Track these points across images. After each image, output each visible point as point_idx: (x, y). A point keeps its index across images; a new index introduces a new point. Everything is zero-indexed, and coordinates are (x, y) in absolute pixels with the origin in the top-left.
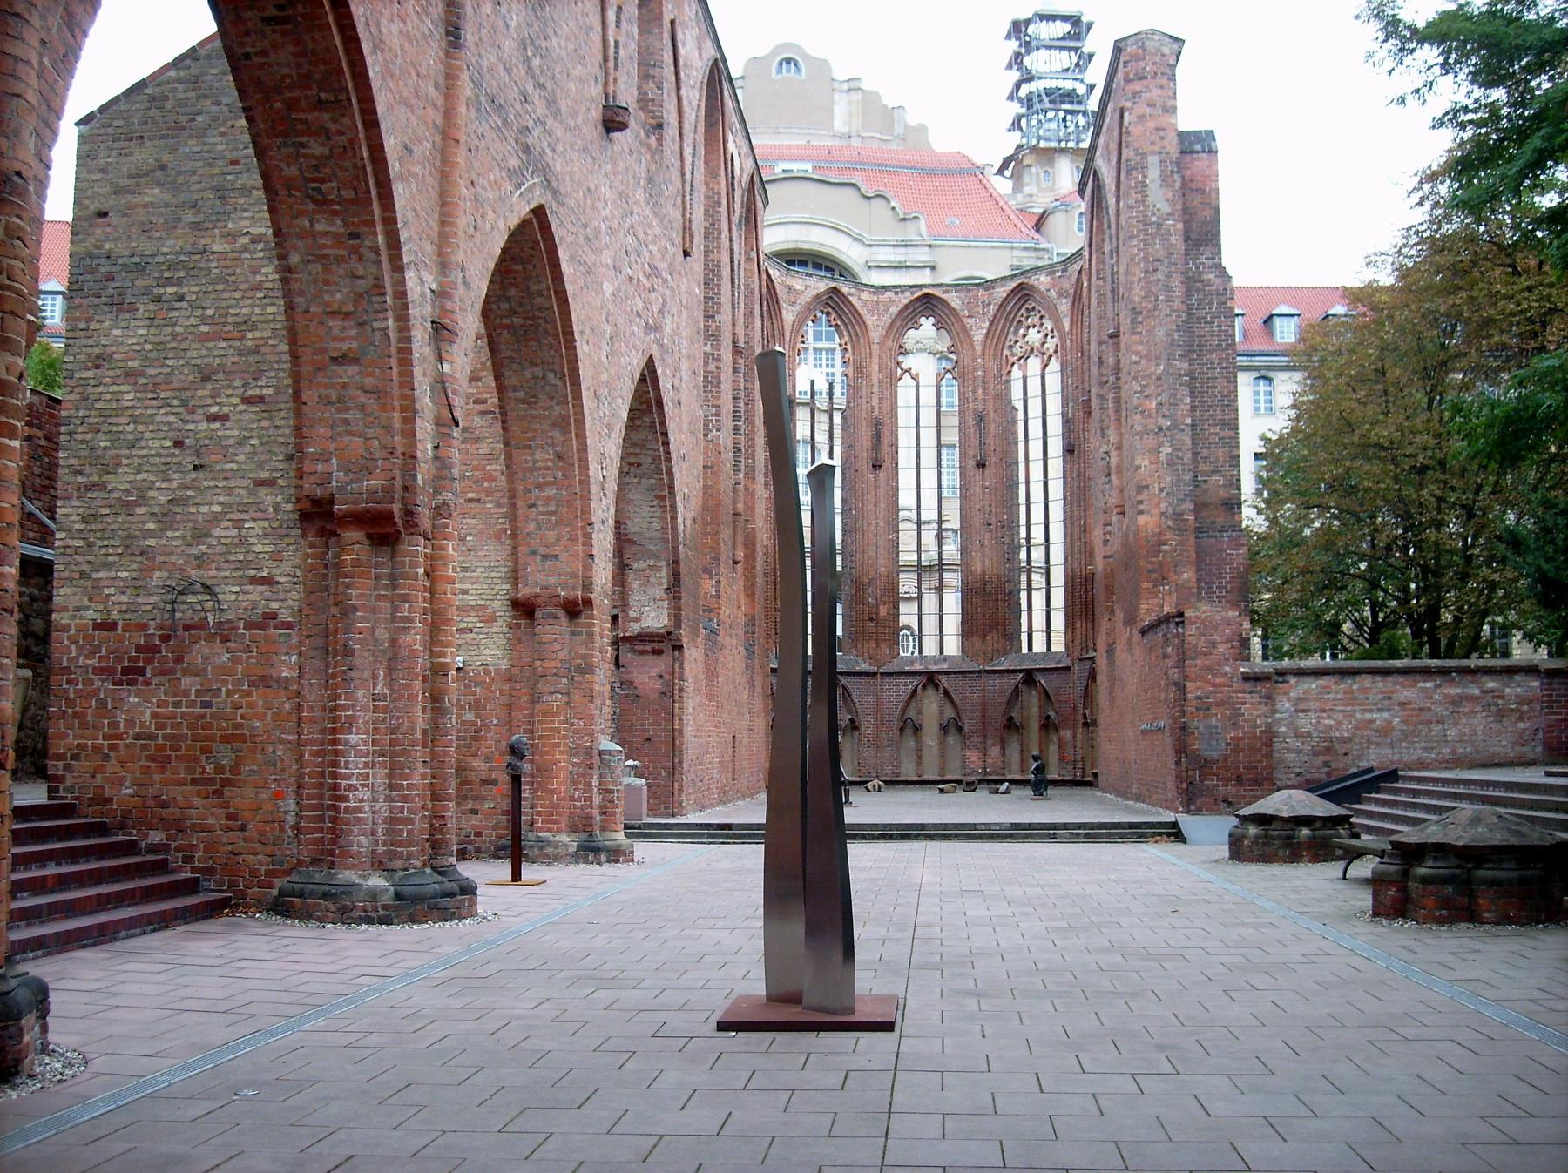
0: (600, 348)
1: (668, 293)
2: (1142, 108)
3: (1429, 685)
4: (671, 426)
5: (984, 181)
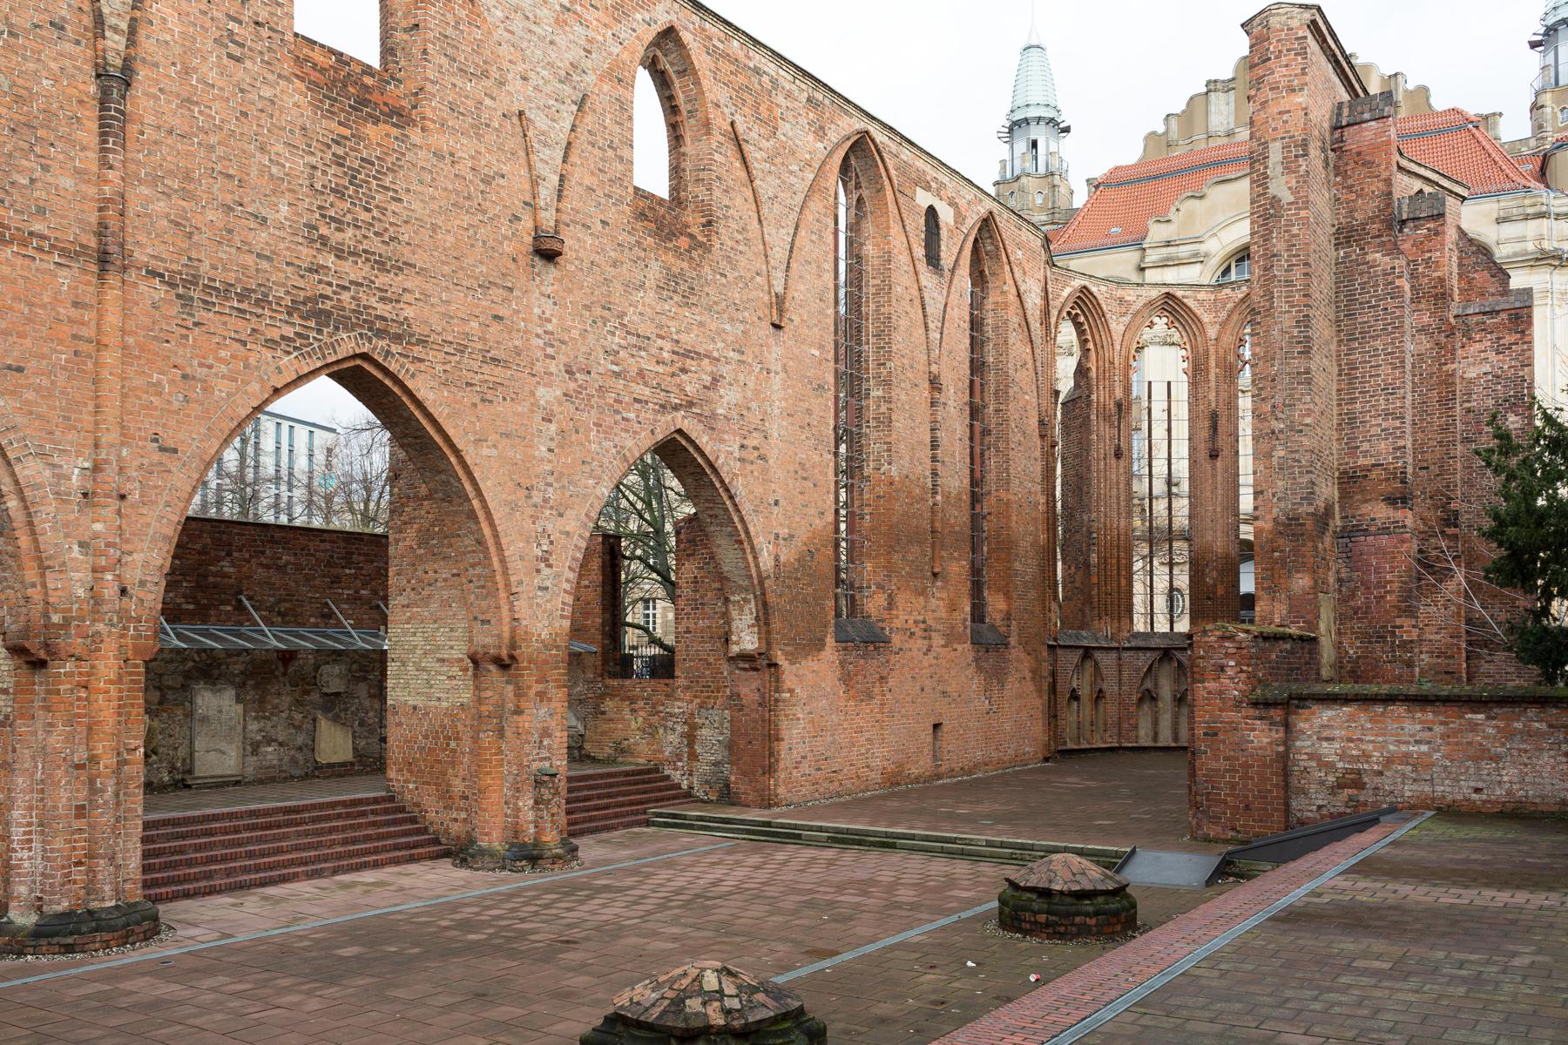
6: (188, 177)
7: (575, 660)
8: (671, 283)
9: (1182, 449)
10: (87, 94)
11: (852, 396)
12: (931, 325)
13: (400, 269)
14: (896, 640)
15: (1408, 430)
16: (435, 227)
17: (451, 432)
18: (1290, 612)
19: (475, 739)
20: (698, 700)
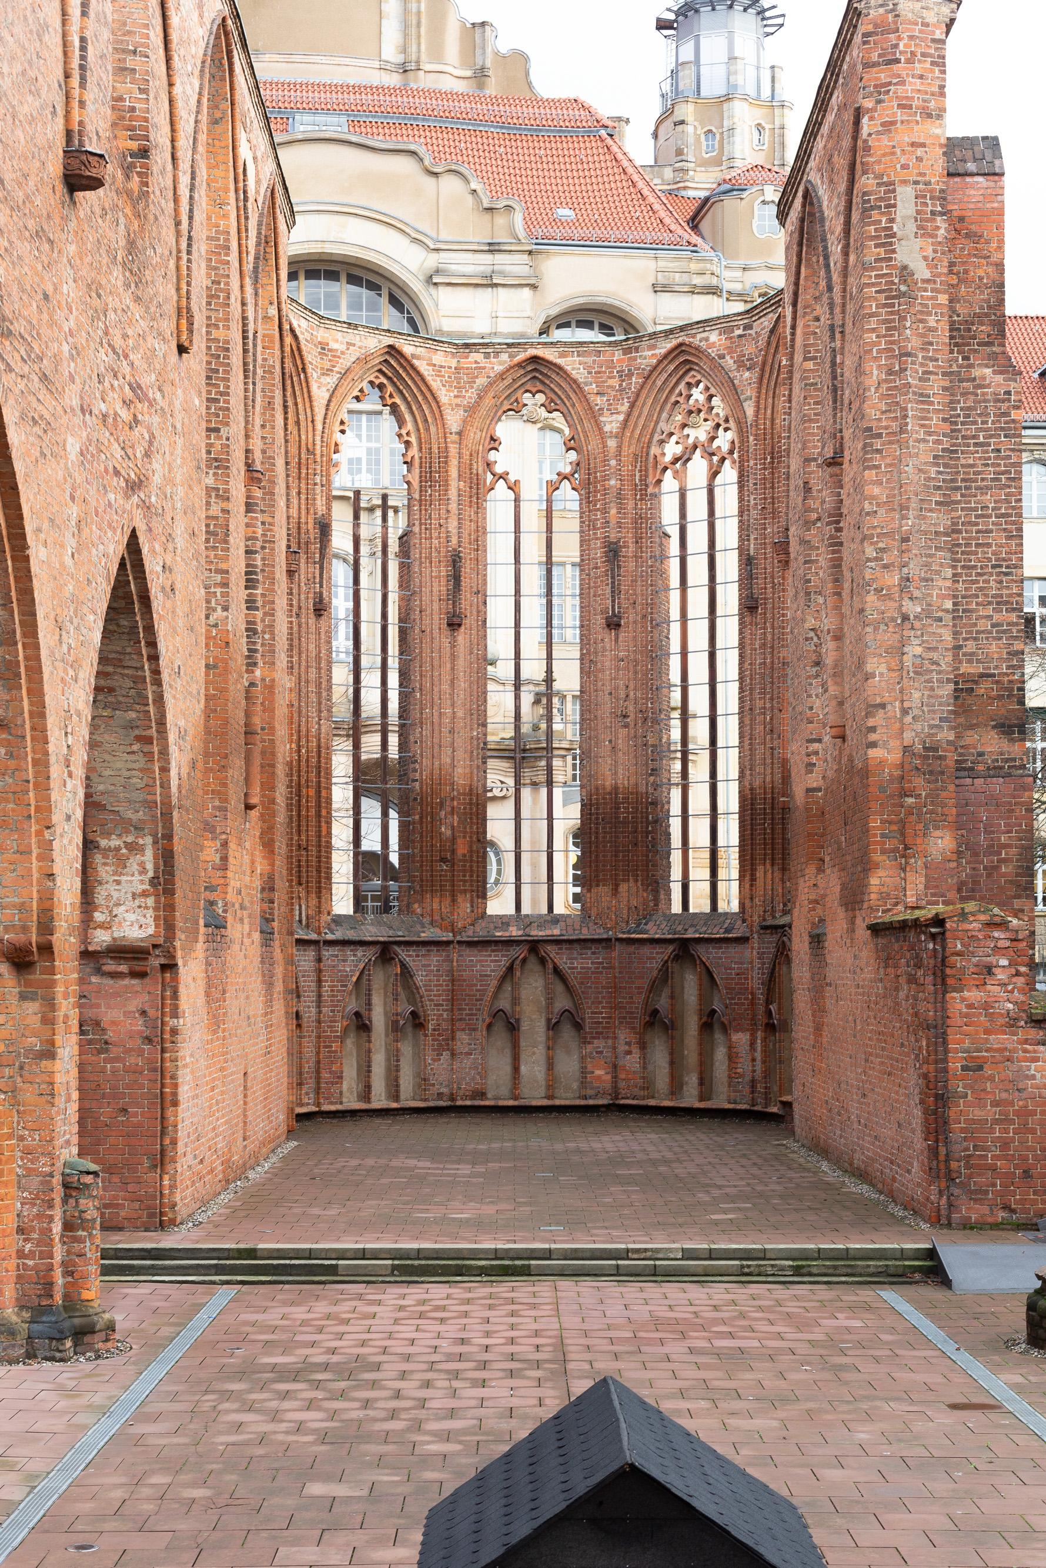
0: (62, 546)
1: (156, 419)
2: (890, 110)
4: (162, 630)
5: (615, 149)
18: (926, 887)
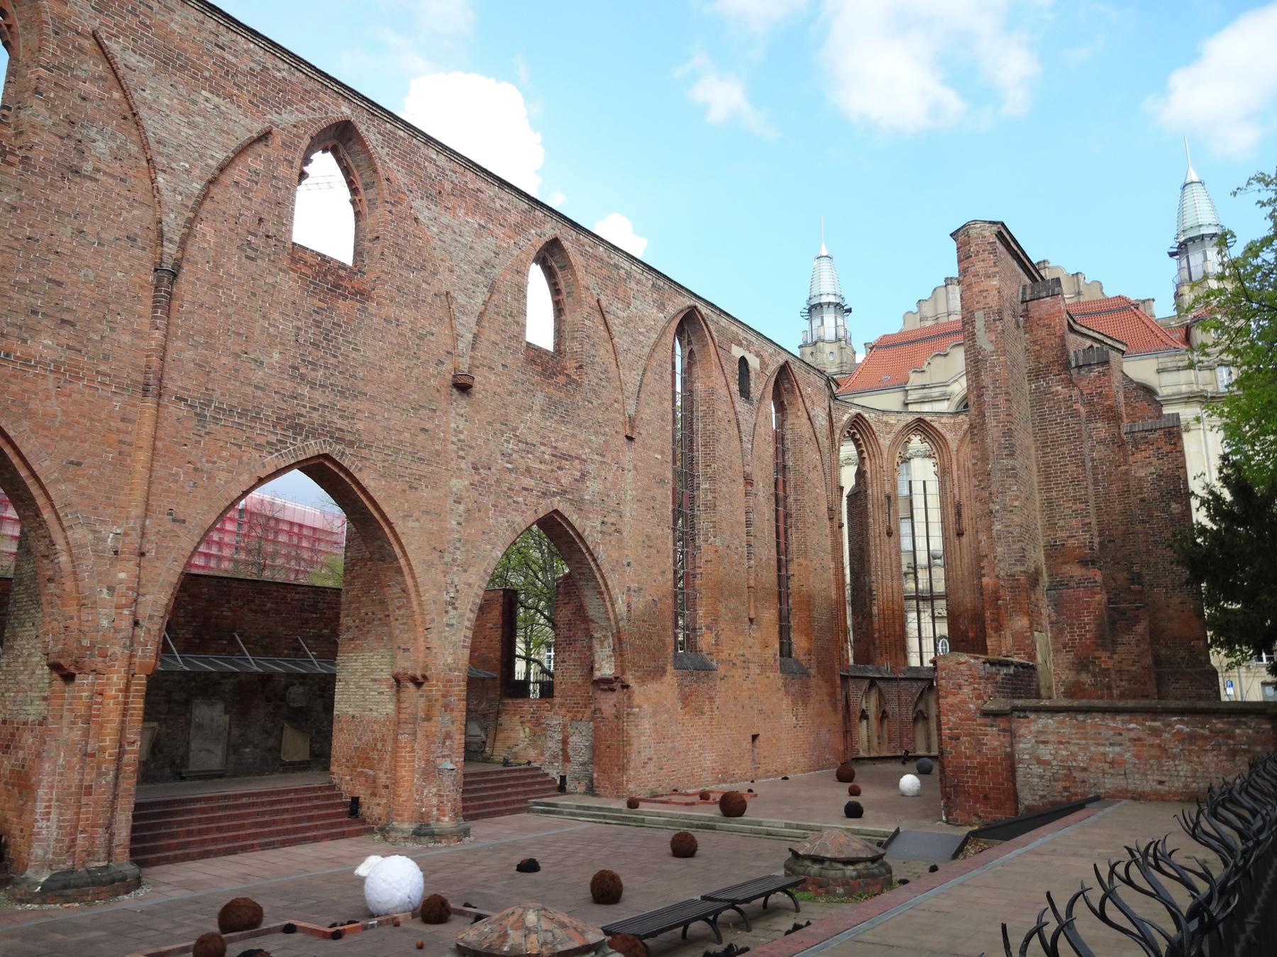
3: (1158, 724)
6: (210, 334)
7: (472, 682)
8: (552, 406)
9: (936, 531)
10: (147, 281)
11: (686, 488)
12: (744, 439)
13: (355, 396)
14: (722, 670)
15: (1092, 510)
16: (382, 369)
17: (385, 509)
19: (396, 740)
20: (571, 714)
